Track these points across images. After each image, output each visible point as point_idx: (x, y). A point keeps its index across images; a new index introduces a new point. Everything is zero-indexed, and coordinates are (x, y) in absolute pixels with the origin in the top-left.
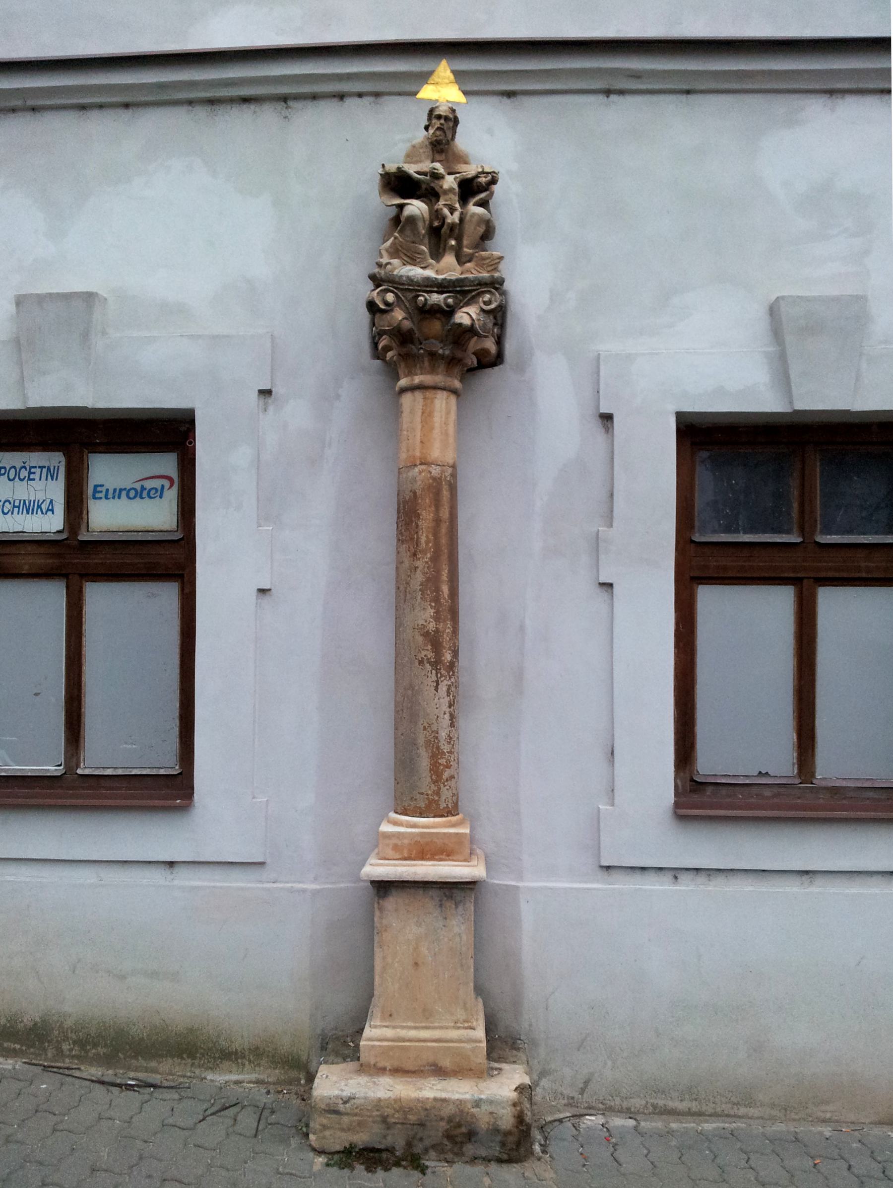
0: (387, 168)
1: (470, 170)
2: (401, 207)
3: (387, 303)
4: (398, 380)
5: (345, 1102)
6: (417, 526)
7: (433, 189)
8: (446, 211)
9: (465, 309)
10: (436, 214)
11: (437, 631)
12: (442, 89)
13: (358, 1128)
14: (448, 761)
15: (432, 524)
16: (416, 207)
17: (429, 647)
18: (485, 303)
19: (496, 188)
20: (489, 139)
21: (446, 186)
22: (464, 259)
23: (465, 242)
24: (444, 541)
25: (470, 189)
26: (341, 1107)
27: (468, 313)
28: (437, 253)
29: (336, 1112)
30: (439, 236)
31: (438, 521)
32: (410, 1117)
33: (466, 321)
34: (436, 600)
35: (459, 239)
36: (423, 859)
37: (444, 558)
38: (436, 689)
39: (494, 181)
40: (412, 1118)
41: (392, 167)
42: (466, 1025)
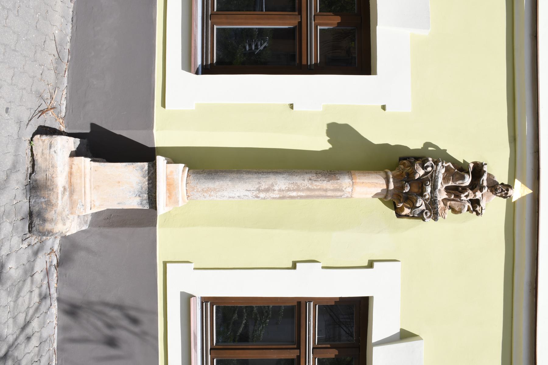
0: (485, 166)
1: (483, 204)
2: (468, 173)
3: (428, 166)
4: (391, 170)
5: (55, 152)
6: (324, 181)
7: (476, 187)
8: (466, 194)
9: (423, 203)
10: (464, 189)
11: (274, 190)
12: (520, 191)
13: (43, 157)
14: (212, 196)
15: (324, 188)
16: (468, 180)
17: (266, 187)
18: (426, 213)
19: (474, 213)
20: (494, 206)
21: (477, 193)
22: (445, 202)
23: (453, 202)
24: (317, 193)
25: (475, 203)
26: (52, 150)
27: (422, 205)
28: (448, 189)
29: (50, 147)
30: (455, 191)
31: (326, 190)
32: (49, 182)
33: (418, 205)
34: (289, 190)
35: (453, 200)
36: (167, 185)
37: (308, 193)
38: (247, 190)
39: (478, 214)
40: (49, 183)
41: (485, 168)
42: (93, 206)
